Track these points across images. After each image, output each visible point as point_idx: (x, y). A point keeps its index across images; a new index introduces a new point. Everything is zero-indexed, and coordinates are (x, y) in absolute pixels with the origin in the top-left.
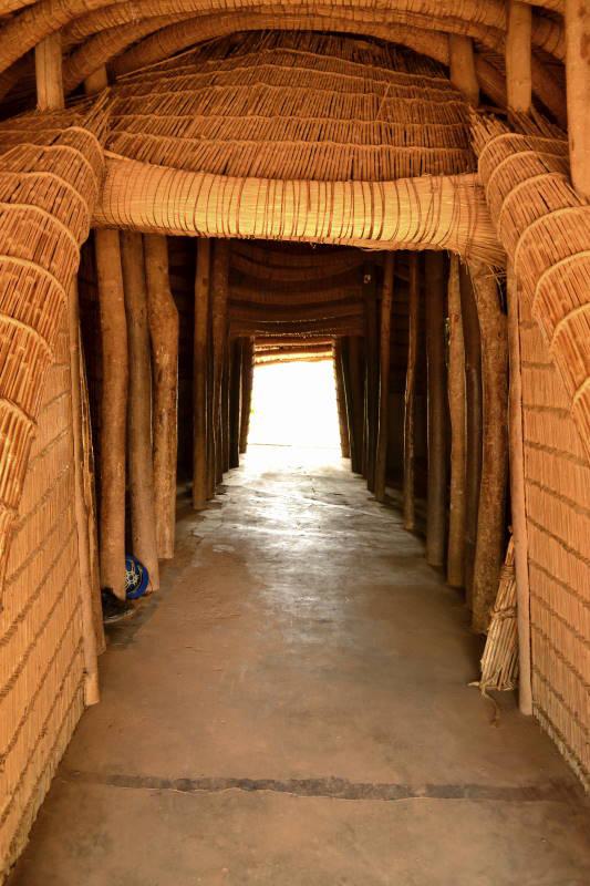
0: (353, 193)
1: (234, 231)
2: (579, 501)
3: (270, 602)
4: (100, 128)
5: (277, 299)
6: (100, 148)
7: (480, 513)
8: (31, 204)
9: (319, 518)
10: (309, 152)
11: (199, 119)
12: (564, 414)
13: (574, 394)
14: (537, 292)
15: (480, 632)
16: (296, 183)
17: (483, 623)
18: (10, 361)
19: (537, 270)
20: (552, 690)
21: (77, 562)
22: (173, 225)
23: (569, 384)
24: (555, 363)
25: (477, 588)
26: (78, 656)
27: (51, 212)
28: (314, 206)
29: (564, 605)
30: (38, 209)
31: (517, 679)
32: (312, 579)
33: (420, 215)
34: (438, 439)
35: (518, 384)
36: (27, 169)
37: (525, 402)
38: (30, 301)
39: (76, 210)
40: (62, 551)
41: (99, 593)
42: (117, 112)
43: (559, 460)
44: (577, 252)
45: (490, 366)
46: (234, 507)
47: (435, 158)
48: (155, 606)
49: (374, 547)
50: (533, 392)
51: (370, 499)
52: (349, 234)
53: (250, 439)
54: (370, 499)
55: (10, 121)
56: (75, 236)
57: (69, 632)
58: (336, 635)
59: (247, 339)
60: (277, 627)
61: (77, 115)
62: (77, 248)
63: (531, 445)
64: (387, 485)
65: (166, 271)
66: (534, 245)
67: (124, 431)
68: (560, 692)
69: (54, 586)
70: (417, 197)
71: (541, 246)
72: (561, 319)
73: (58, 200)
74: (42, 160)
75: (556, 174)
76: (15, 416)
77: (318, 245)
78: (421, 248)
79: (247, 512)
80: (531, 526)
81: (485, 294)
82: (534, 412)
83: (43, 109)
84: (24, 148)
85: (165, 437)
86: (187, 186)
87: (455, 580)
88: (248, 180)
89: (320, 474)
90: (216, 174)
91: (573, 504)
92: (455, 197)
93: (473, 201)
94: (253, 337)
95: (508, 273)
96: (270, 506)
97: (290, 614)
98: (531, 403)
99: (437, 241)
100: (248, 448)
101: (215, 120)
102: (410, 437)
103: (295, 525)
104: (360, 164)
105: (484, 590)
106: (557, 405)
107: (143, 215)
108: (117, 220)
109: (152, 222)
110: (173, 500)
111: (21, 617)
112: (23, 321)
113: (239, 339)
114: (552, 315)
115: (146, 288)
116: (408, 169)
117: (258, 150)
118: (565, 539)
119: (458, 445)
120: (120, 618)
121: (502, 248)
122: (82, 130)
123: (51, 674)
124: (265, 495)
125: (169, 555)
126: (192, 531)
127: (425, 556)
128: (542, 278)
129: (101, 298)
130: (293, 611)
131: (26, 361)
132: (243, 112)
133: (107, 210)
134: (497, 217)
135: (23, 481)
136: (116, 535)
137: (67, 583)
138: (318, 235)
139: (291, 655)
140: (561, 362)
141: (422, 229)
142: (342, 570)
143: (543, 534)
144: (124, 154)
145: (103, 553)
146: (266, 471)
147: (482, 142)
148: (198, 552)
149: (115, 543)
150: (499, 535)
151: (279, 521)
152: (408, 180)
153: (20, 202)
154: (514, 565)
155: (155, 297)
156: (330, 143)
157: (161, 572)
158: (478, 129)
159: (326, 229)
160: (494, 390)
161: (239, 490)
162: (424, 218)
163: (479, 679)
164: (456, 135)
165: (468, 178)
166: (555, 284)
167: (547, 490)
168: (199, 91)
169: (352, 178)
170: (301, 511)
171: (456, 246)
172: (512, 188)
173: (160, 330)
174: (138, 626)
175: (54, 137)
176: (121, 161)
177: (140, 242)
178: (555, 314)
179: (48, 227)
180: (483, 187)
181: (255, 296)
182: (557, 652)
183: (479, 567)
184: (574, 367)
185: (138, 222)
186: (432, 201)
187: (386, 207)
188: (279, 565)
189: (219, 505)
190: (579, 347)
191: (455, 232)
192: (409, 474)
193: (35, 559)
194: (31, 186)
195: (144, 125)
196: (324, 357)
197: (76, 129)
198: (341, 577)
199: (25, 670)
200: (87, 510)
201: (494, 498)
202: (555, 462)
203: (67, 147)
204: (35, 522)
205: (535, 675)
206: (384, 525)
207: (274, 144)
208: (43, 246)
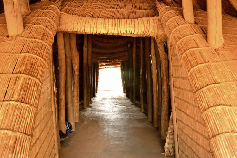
0: (127, 22)
1: (95, 32)
2: (190, 102)
3: (106, 133)
4: (59, 6)
5: (105, 51)
6: (59, 10)
7: (162, 106)
8: (41, 25)
9: (118, 110)
10: (114, 12)
11: (85, 3)
12: (184, 78)
13: (188, 73)
14: (177, 46)
15: (163, 139)
16: (112, 19)
17: (164, 137)
18: (36, 67)
19: (176, 41)
20: (184, 154)
21: (53, 123)
22: (79, 31)
23: (187, 70)
24: (183, 65)
25: (162, 126)
26: (53, 150)
27: (46, 27)
28: (116, 25)
29: (186, 130)
30: (42, 26)
31: (174, 152)
32: (117, 126)
33: (144, 27)
34: (150, 87)
35: (171, 71)
36: (39, 16)
37: (174, 76)
38: (41, 51)
40: (48, 120)
41: (58, 132)
43: (184, 91)
44: (186, 36)
45: (163, 67)
46: (95, 107)
47: (147, 13)
48: (74, 135)
49: (134, 117)
50: (176, 73)
51: (131, 104)
52: (126, 33)
53: (99, 89)
54: (131, 104)
55: (34, 4)
56: (53, 33)
57: (51, 143)
58: (124, 141)
59: (97, 62)
60: (108, 140)
61: (52, 2)
62: (53, 37)
63: (176, 87)
64: (136, 100)
65: (76, 44)
66: (175, 34)
67: (65, 87)
68: (187, 154)
69: (47, 130)
70: (143, 23)
71: (177, 34)
72: (183, 53)
74: (43, 14)
75: (180, 16)
77: (118, 36)
78: (144, 36)
79: (98, 109)
80: (176, 109)
81: (161, 49)
82: (176, 79)
86: (82, 20)
87: (156, 125)
89: (118, 98)
90: (90, 17)
91: (188, 103)
92: (153, 22)
93: (158, 24)
94: (99, 62)
95: (168, 42)
96: (105, 107)
97: (112, 136)
98: (175, 76)
99: (149, 34)
100: (98, 91)
101: (89, 4)
102: (142, 87)
103: (112, 112)
105: (164, 127)
106: (182, 76)
107: (71, 28)
108: (64, 30)
110: (78, 105)
111: (38, 139)
112: (39, 56)
113: (95, 62)
114: (181, 52)
115: (70, 49)
116: (140, 16)
117: (101, 11)
118: (186, 112)
119: (155, 89)
120: (64, 139)
121: (166, 35)
122: (54, 6)
123: (46, 155)
124: (103, 104)
125: (77, 121)
127: (147, 119)
128: (178, 43)
129: (58, 51)
130: (112, 135)
131: (40, 67)
133: (61, 27)
134: (165, 28)
135: (39, 100)
136: (63, 116)
137: (50, 129)
138: (118, 33)
139: (112, 147)
140: (184, 64)
142: (125, 123)
143: (180, 111)
144: (65, 12)
145: (60, 121)
146: (103, 97)
147: (160, 9)
148: (85, 120)
149: (63, 118)
150: (167, 112)
151: (107, 111)
152: (141, 18)
153: (38, 24)
154: (172, 120)
155: (73, 51)
156: (120, 9)
157: (75, 126)
158: (158, 5)
159: (120, 31)
160: (165, 73)
161: (96, 103)
162: (145, 28)
163: (164, 152)
164: (152, 7)
165: (157, 18)
166: (181, 44)
167: (181, 99)
169: (126, 18)
170: (113, 108)
171: (153, 35)
172: (168, 20)
173: (74, 60)
174: (69, 141)
175: (46, 8)
176: (64, 14)
177: (69, 36)
178: (182, 52)
179: (45, 31)
180: (160, 20)
181: (100, 51)
182: (185, 143)
183: (163, 121)
184: (188, 65)
185: (69, 30)
186: (147, 24)
188: (108, 123)
189: (91, 107)
190: (189, 60)
191: (154, 31)
192: (142, 96)
193: (41, 122)
194: (41, 20)
195: (70, 5)
196: (118, 67)
197: (52, 6)
198: (125, 125)
199: (39, 154)
200: (55, 108)
201: (166, 102)
202: (183, 92)
203: (50, 10)
204: (41, 112)
205: (179, 149)
206: (136, 111)
207: (105, 10)
208: (44, 36)
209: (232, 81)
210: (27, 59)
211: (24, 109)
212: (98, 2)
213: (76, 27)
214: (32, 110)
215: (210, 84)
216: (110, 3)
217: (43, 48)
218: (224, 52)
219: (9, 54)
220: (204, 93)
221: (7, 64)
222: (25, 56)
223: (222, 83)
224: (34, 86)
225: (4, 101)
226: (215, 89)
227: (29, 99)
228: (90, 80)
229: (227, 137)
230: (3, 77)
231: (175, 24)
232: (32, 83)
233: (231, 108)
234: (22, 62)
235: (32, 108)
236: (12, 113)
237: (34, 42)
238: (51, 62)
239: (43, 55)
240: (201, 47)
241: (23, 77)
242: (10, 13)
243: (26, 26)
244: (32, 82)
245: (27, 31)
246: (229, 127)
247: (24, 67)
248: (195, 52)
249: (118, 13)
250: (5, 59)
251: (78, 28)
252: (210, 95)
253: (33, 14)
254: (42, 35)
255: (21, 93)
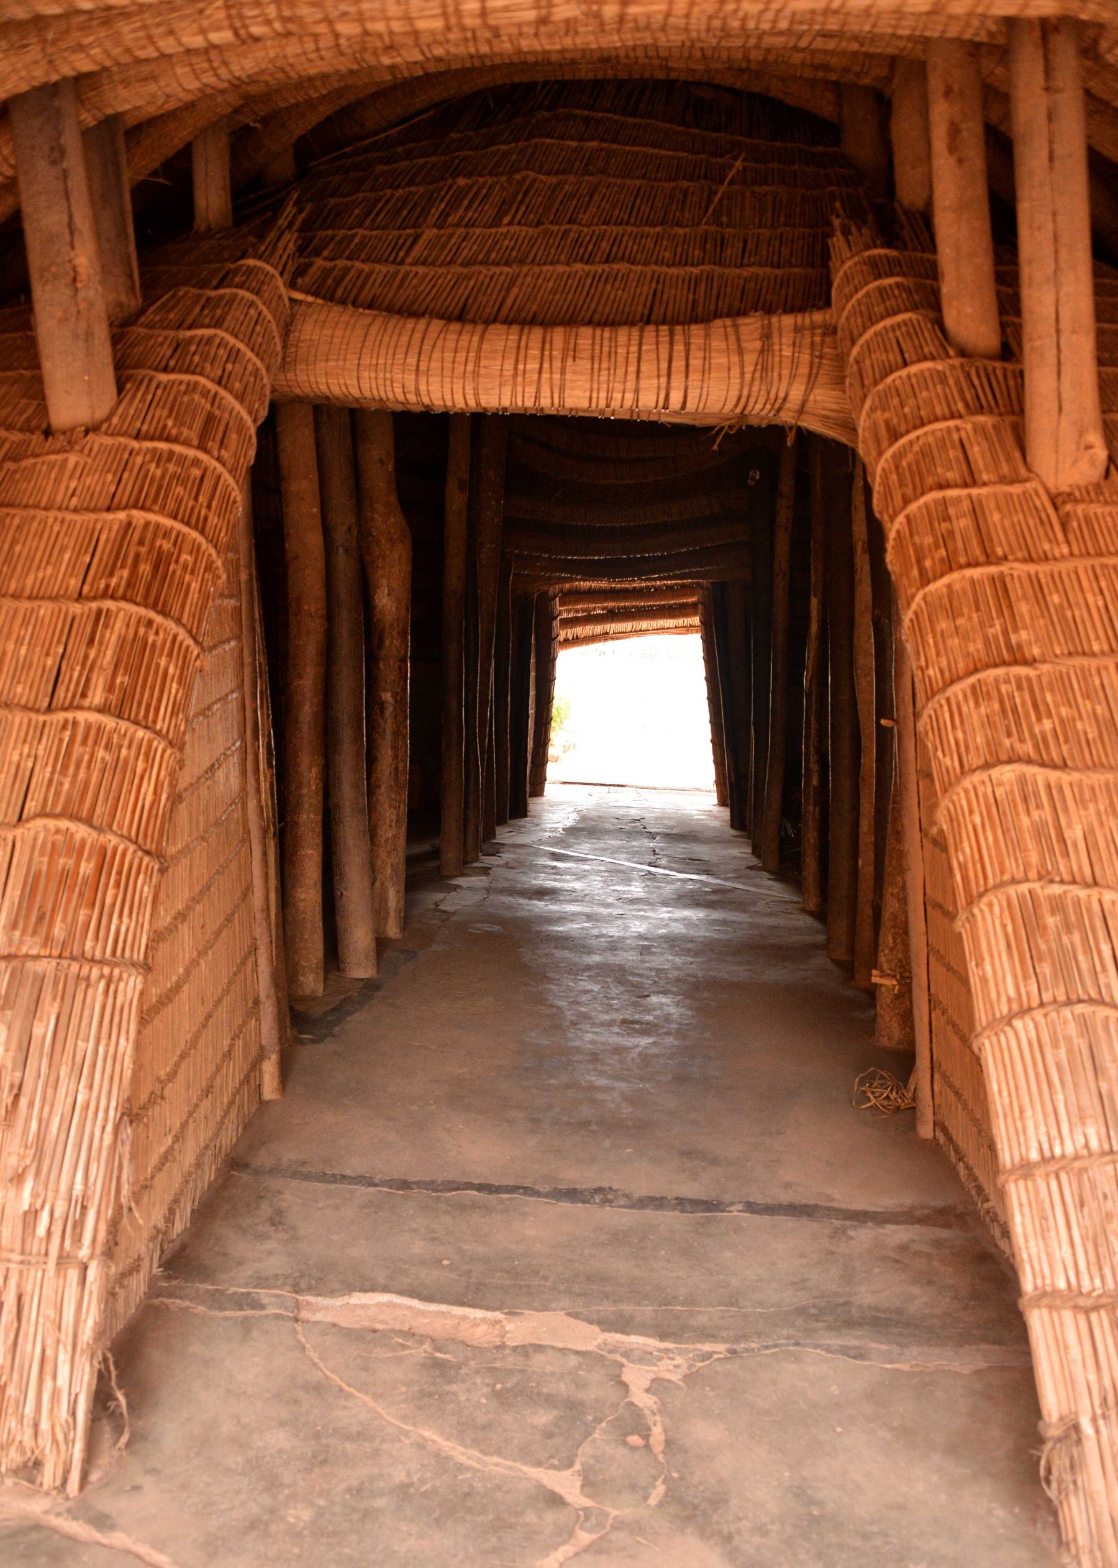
1: (520, 403)
4: (284, 258)
6: (283, 289)
8: (193, 373)
10: (589, 281)
11: (429, 233)
27: (219, 383)
30: (203, 380)
33: (742, 374)
38: (196, 498)
39: (252, 379)
42: (306, 227)
61: (252, 239)
62: (253, 431)
65: (390, 467)
66: (879, 413)
71: (887, 415)
73: (229, 366)
74: (206, 312)
76: (179, 638)
83: (203, 228)
84: (181, 293)
85: (389, 736)
86: (405, 339)
88: (491, 327)
101: (451, 236)
104: (665, 296)
109: (412, 398)
112: (188, 524)
125: (393, 930)
126: (437, 904)
132: (496, 222)
141: (745, 393)
144: (316, 294)
153: (180, 371)
158: (837, 242)
159: (603, 395)
162: (748, 376)
168: (432, 187)
176: (310, 305)
187: (691, 362)
194: (193, 348)
197: (251, 262)
205: (936, 1076)
209: (1103, 653)
210: (136, 536)
211: (130, 747)
212: (506, 220)
213: (373, 375)
214: (162, 757)
215: (987, 666)
216: (575, 227)
217: (208, 485)
218: (1099, 511)
219: (60, 515)
220: (954, 708)
221: (53, 559)
222: (129, 524)
223: (1044, 662)
224: (170, 655)
225: (49, 709)
226: (1004, 688)
227: (148, 705)
228: (484, 704)
229: (1015, 902)
230: (42, 612)
231: (891, 357)
232: (159, 643)
233: (1059, 779)
234: (121, 546)
235: (159, 745)
236: (86, 757)
237: (164, 459)
238: (242, 563)
239: (206, 518)
240: (984, 484)
241: (121, 614)
242: (60, 321)
243: (127, 381)
244: (161, 636)
245: (134, 406)
246: (1034, 858)
247: (126, 573)
248: (952, 511)
249: (609, 288)
250: (46, 535)
251: (381, 382)
252: (975, 717)
253: (156, 312)
254: (198, 424)
255: (118, 681)
